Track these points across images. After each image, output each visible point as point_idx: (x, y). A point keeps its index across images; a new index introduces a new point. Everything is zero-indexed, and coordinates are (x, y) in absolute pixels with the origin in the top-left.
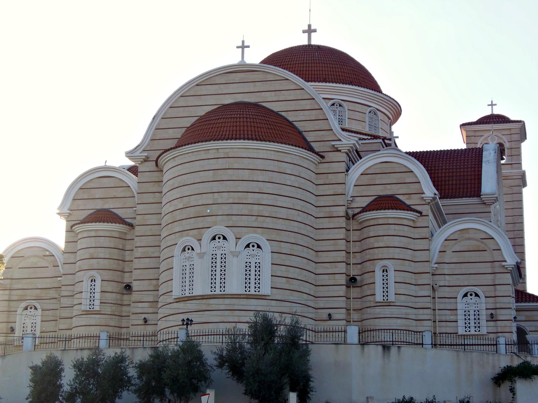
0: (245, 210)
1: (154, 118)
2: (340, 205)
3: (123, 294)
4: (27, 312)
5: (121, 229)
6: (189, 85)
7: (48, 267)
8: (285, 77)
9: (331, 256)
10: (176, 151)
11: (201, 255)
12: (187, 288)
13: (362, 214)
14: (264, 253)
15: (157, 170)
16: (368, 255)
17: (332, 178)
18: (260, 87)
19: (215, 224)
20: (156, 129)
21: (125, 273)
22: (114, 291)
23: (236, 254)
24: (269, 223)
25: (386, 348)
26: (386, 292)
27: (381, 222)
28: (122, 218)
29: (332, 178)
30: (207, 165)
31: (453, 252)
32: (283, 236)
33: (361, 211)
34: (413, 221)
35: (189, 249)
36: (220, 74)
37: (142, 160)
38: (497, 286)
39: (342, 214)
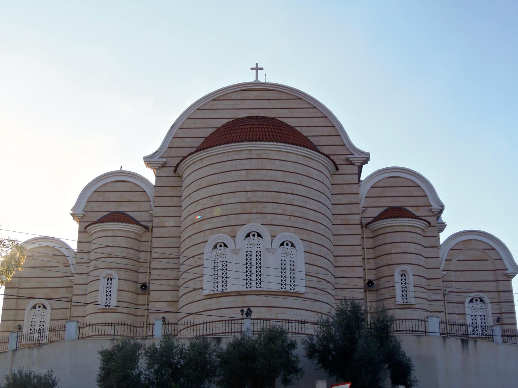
0: (279, 209)
1: (172, 127)
2: (356, 213)
3: (138, 294)
4: (36, 311)
5: (137, 230)
6: (208, 98)
7: (58, 267)
8: (298, 97)
9: (349, 261)
10: (204, 152)
11: (236, 252)
12: (220, 285)
13: (375, 223)
14: (298, 252)
15: (174, 176)
16: (386, 260)
17: (346, 189)
18: (274, 104)
19: (250, 221)
20: (173, 138)
21: (140, 274)
22: (130, 291)
23: (271, 252)
24: (301, 223)
25: (464, 343)
26: (405, 296)
27: (397, 229)
28: (137, 221)
29: (346, 189)
30: (239, 165)
31: (457, 261)
32: (314, 237)
33: (372, 221)
34: (423, 230)
35: (221, 246)
36: (236, 91)
37: (160, 165)
38: (501, 293)
39: (359, 222)
